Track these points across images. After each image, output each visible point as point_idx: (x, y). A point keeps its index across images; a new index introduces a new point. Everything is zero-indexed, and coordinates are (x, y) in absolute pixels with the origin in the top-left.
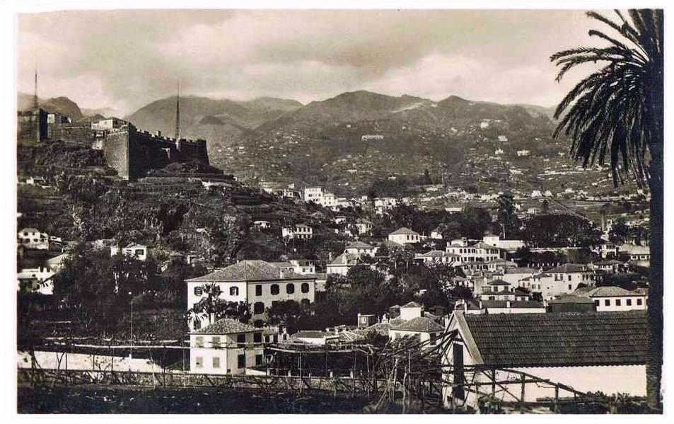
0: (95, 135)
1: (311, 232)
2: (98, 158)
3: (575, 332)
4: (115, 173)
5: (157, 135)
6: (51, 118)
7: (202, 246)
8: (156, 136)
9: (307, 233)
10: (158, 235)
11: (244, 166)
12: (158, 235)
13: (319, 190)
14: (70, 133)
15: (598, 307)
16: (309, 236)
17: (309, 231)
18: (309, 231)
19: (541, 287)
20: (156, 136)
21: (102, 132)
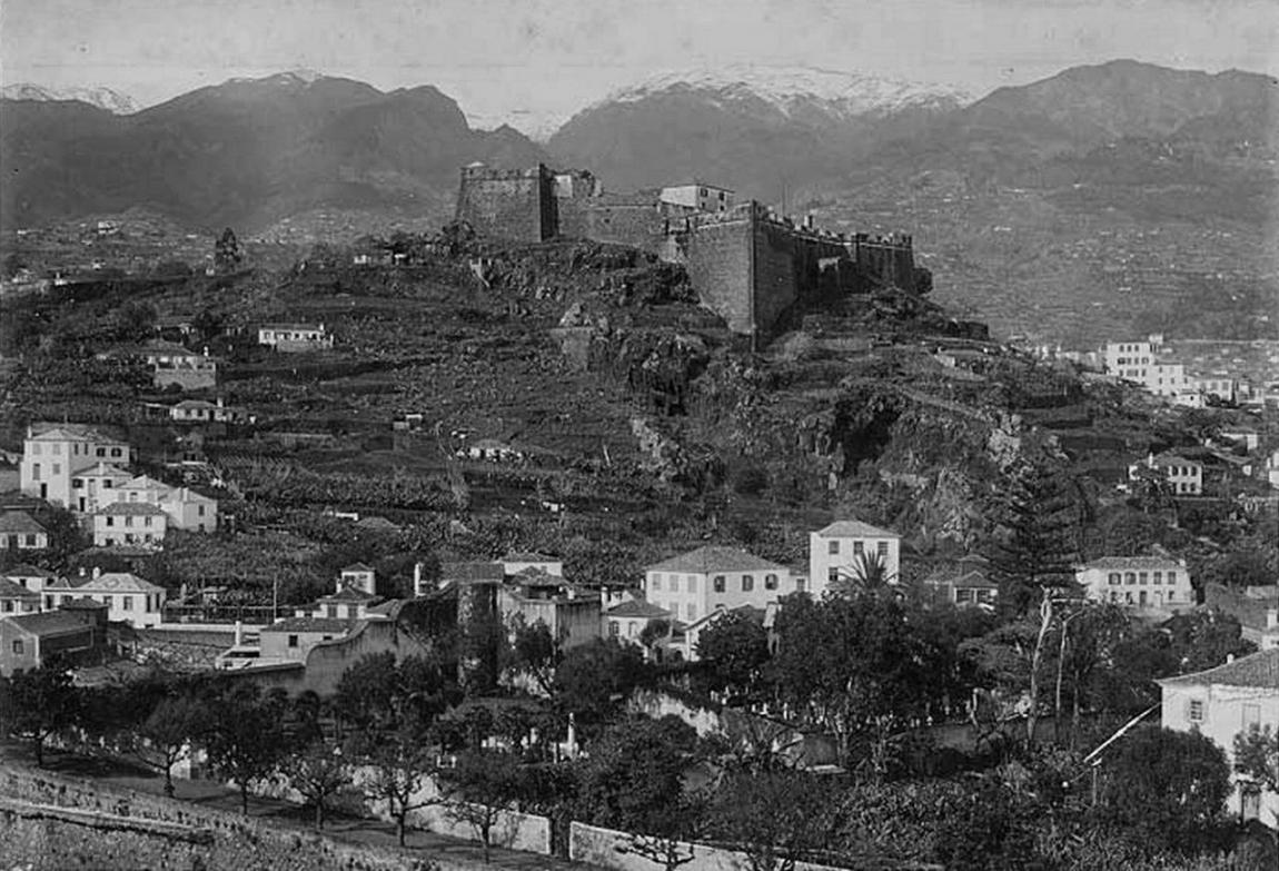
0: (667, 227)
1: (1198, 479)
2: (671, 287)
3: (622, 847)
4: (722, 323)
5: (806, 223)
6: (564, 183)
7: (941, 507)
8: (804, 228)
9: (1189, 479)
10: (832, 476)
11: (1093, 322)
12: (832, 476)
13: (116, 112)
14: (607, 221)
15: (288, 697)
16: (1193, 487)
17: (1194, 473)
18: (1194, 473)
19: (197, 511)
20: (804, 228)
21: (684, 221)
